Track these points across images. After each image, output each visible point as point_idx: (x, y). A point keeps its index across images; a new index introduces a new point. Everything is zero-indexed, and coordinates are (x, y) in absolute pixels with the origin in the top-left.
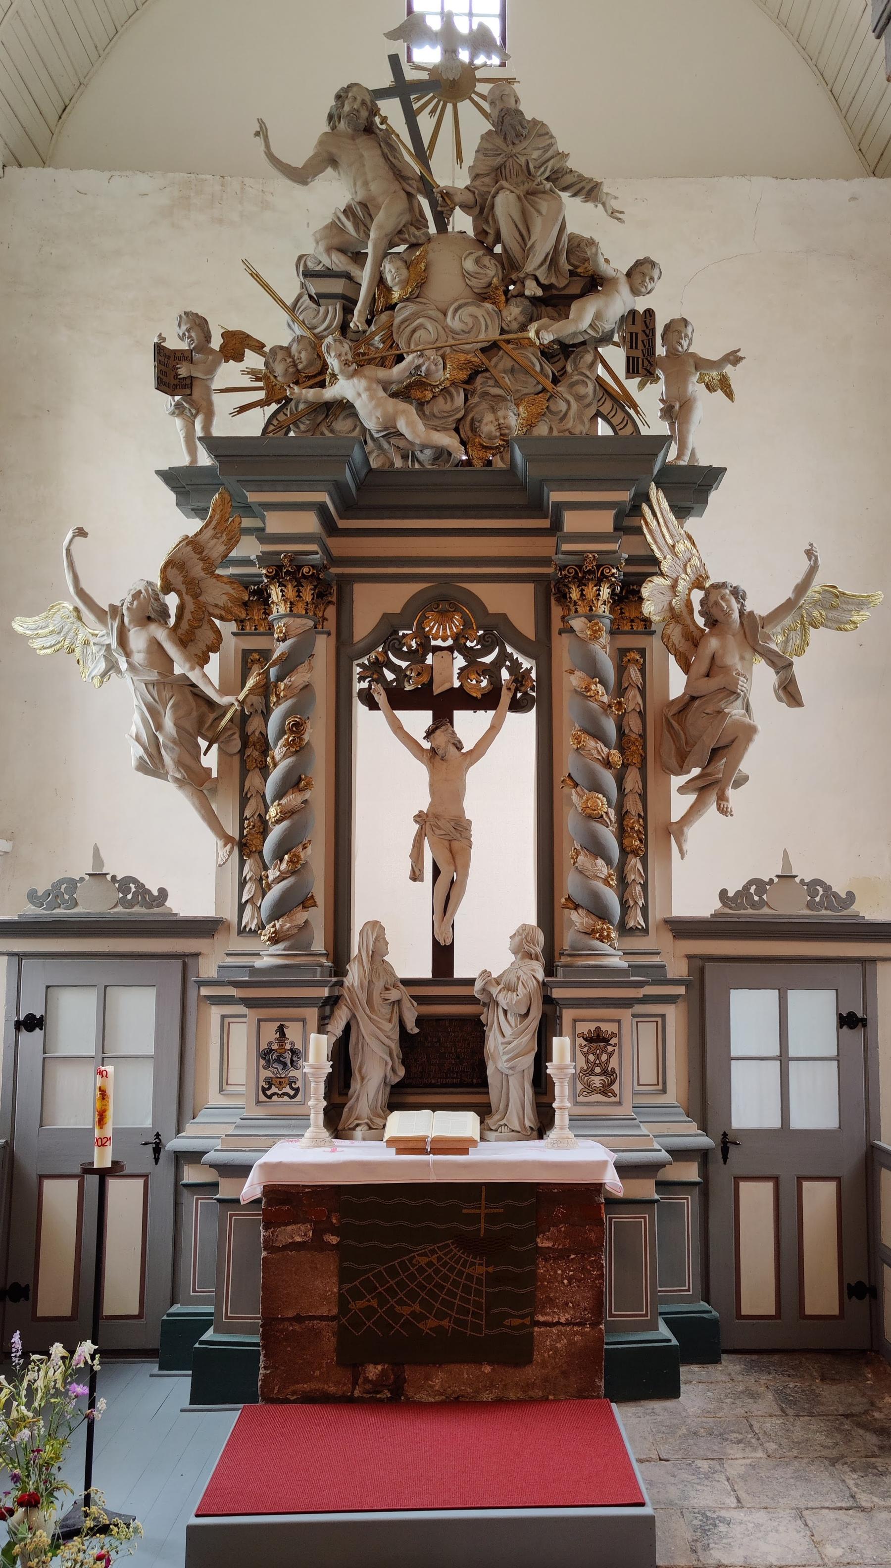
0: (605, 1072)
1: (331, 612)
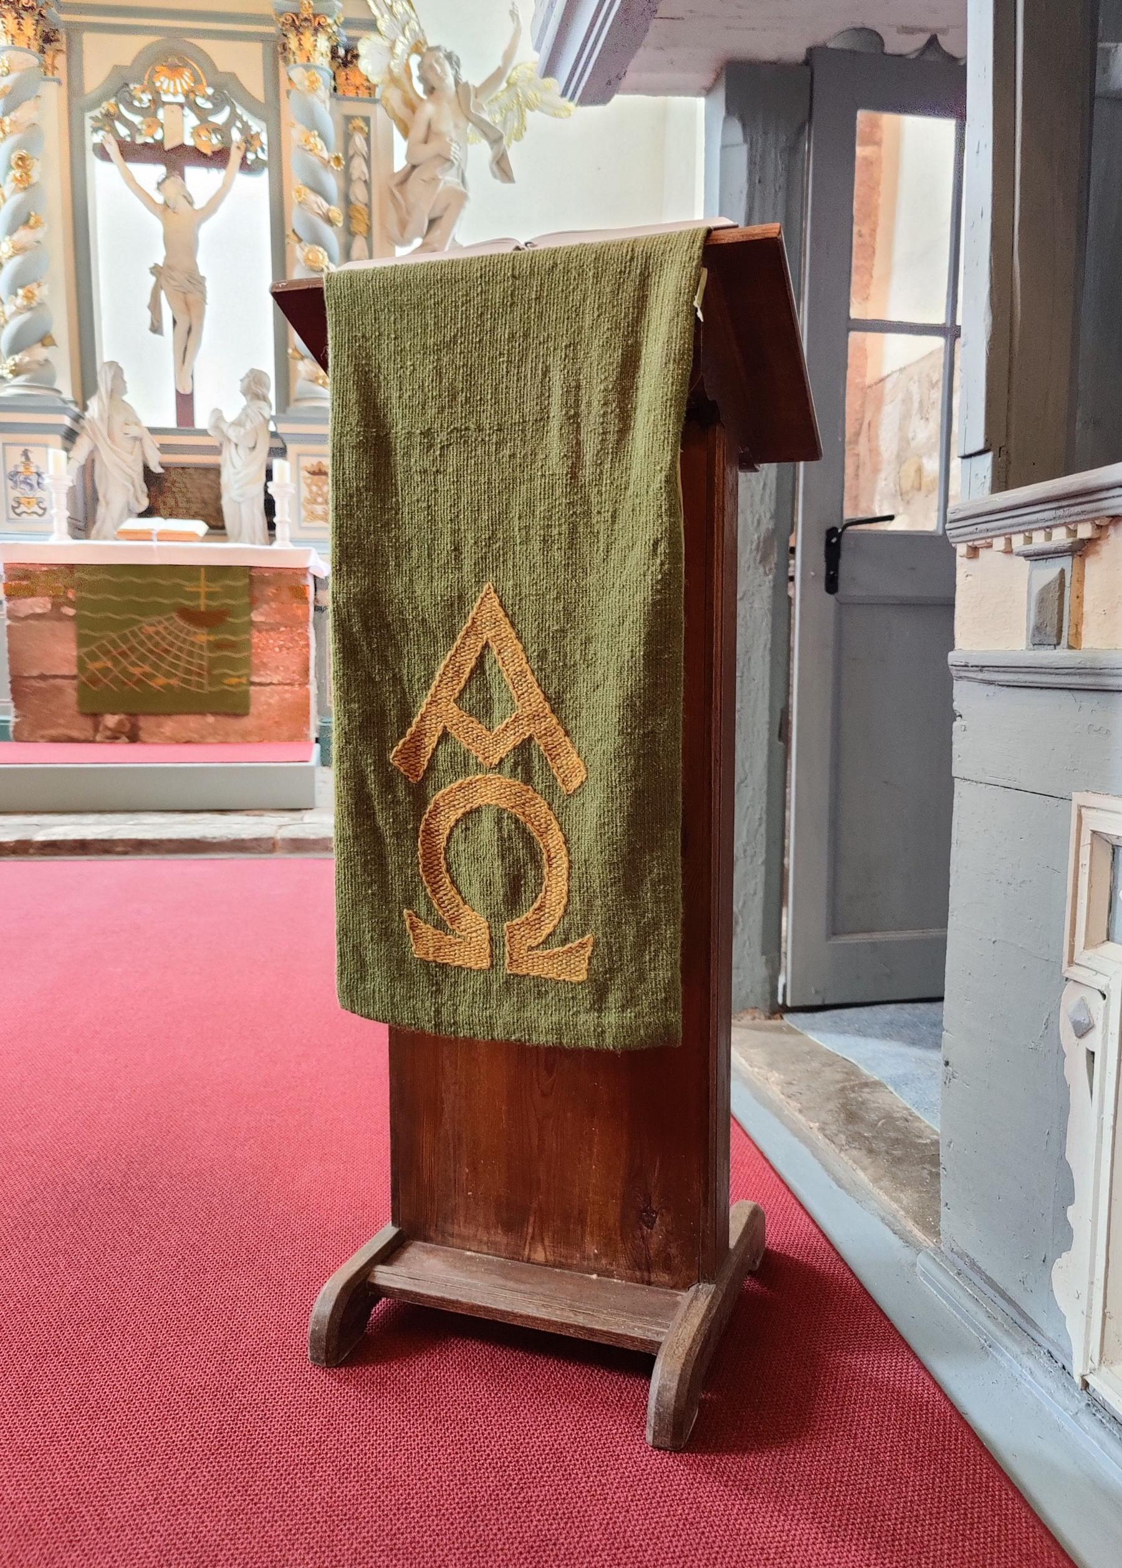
1: (61, 60)
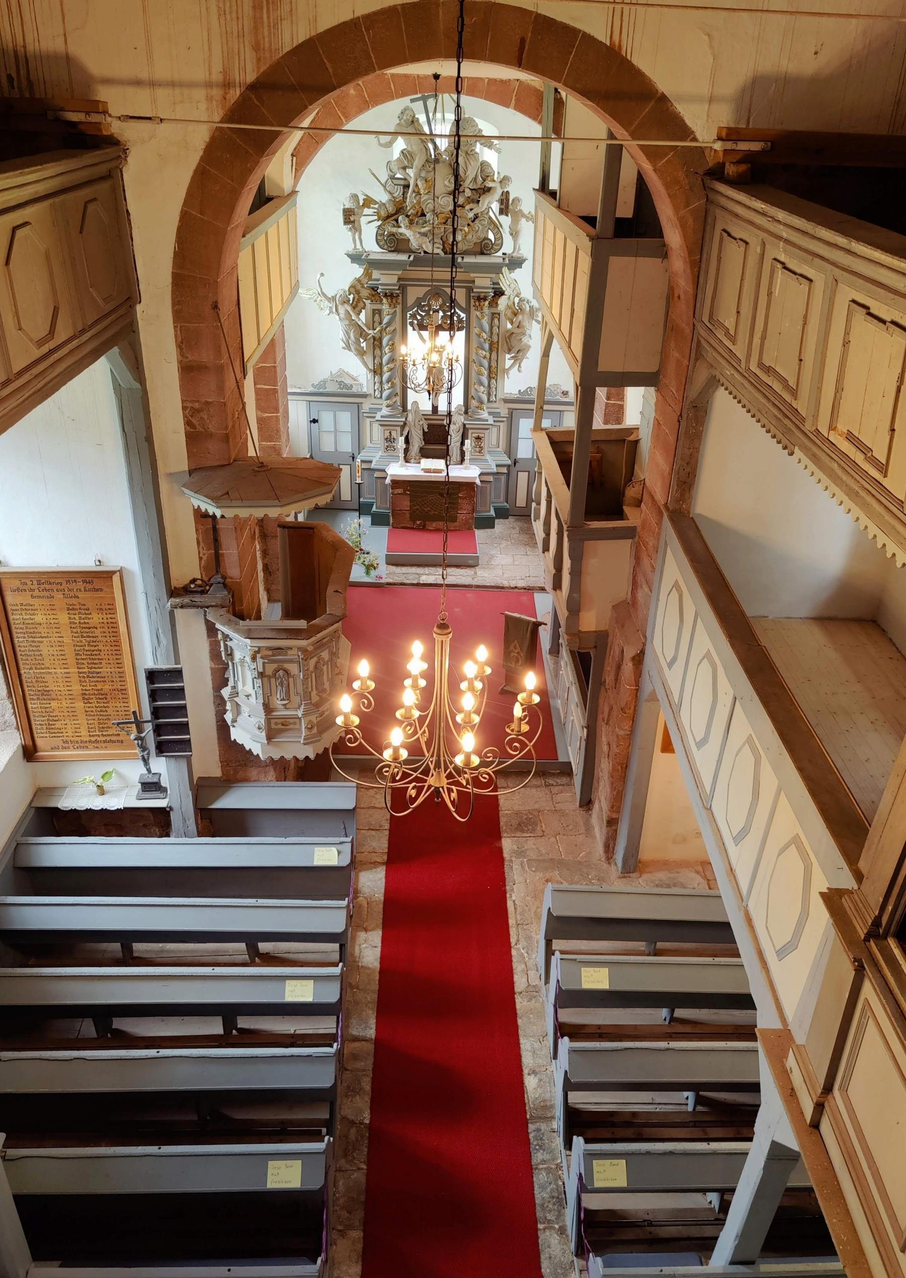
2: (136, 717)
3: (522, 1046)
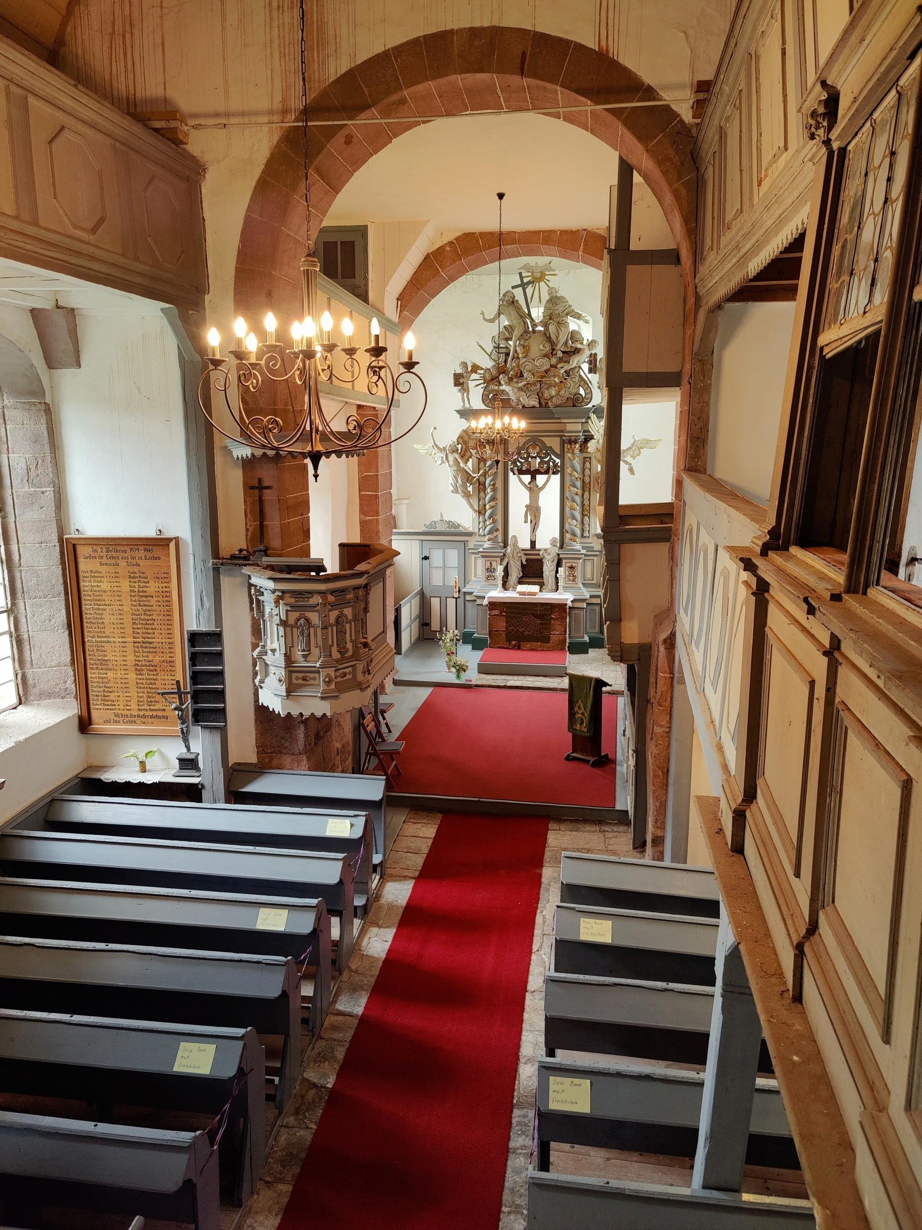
0: (573, 576)
2: (179, 688)
3: (523, 1038)
